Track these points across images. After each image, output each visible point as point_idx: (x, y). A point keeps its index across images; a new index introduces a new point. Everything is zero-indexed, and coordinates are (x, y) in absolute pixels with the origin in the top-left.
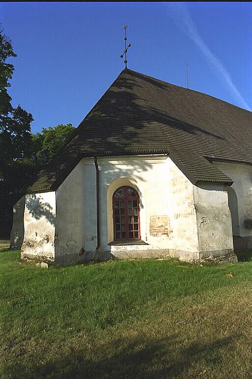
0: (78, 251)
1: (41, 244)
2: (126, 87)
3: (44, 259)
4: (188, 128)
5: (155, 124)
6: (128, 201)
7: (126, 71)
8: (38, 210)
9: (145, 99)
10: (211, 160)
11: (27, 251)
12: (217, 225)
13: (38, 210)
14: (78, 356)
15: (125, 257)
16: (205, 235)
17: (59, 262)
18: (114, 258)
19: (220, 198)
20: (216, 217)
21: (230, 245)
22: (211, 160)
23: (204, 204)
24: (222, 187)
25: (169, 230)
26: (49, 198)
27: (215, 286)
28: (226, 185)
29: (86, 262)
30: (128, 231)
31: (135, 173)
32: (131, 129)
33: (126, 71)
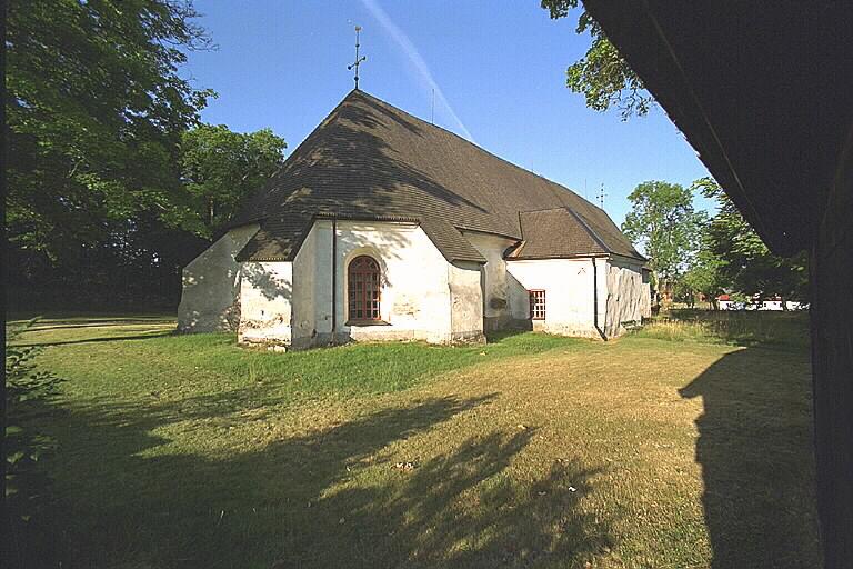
0: (311, 333)
1: (270, 324)
2: (367, 124)
3: (276, 342)
4: (450, 198)
5: (410, 188)
6: (366, 275)
7: (356, 96)
8: (20, 227)
9: (398, 149)
10: (463, 231)
11: (249, 333)
12: (469, 305)
13: (267, 286)
14: (426, 428)
15: (365, 339)
16: (457, 315)
17: (295, 344)
18: (351, 340)
19: (470, 278)
20: (469, 298)
21: (480, 327)
22: (463, 231)
23: (457, 283)
24: (476, 266)
25: (415, 308)
26: (282, 271)
27: (473, 362)
28: (479, 265)
29: (323, 346)
30: (365, 311)
31: (391, 249)
32: (382, 191)
33: (356, 96)
